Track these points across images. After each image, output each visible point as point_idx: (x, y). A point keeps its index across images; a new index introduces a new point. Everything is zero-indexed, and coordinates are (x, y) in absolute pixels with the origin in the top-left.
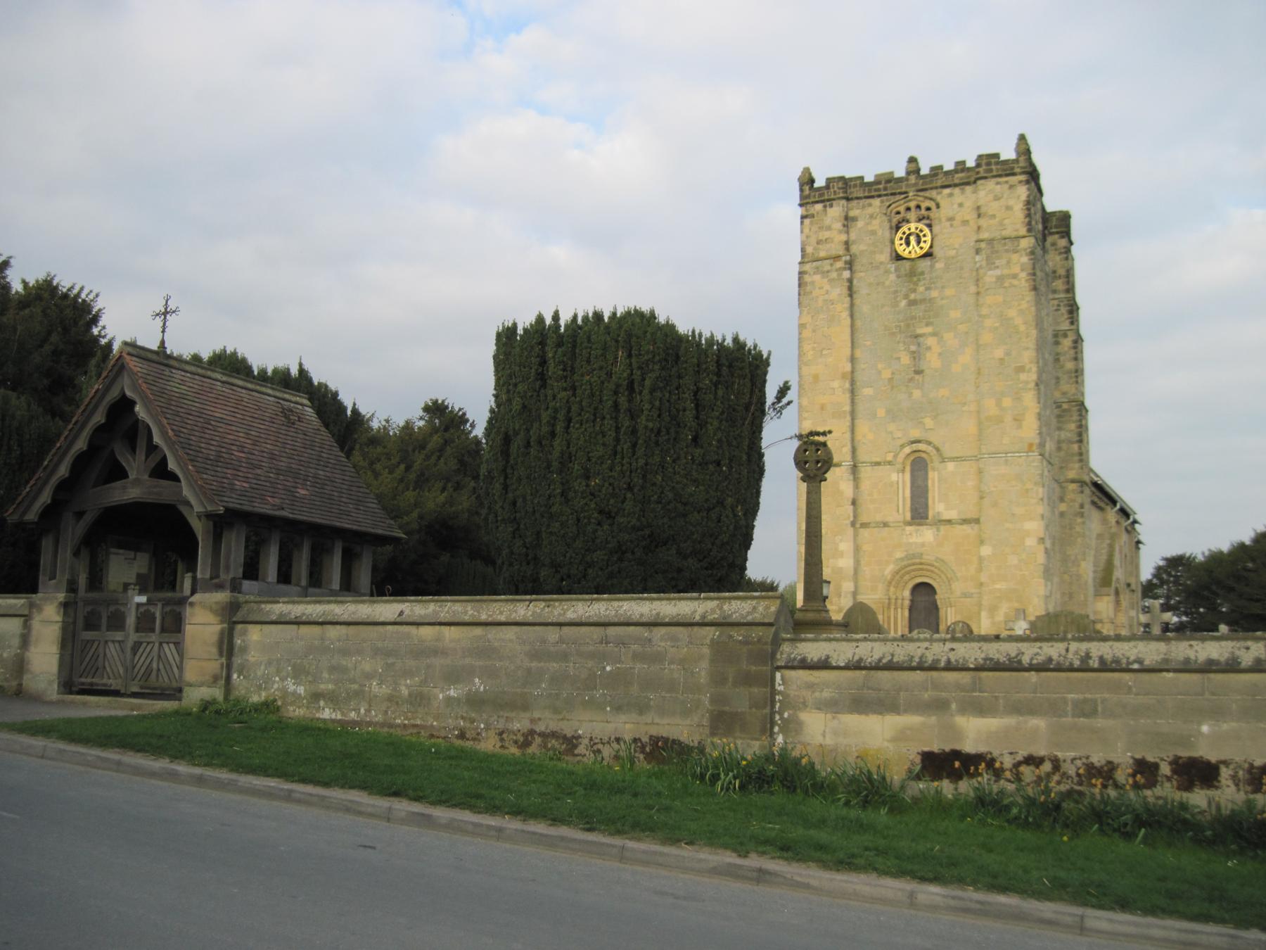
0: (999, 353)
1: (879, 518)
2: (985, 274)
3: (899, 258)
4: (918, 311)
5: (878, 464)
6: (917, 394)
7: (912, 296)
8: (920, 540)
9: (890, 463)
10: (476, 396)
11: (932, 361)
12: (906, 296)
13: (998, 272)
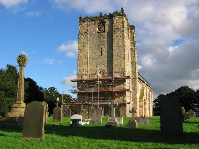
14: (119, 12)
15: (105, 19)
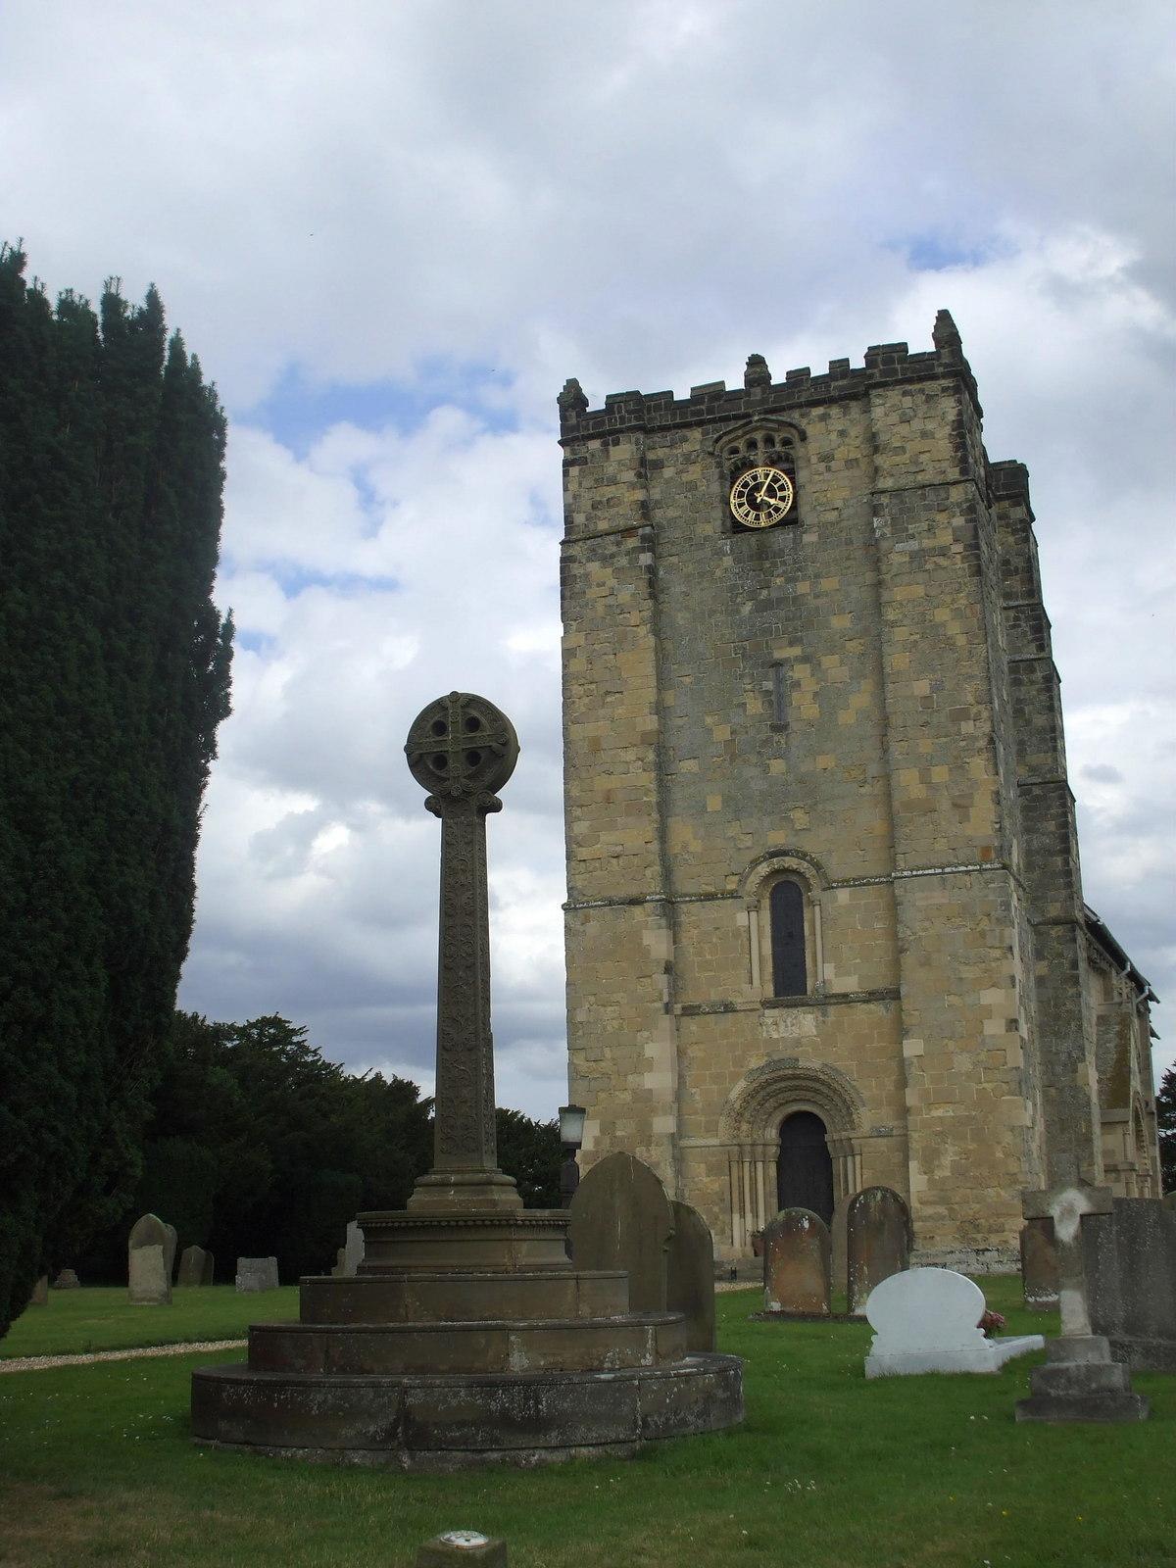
3: (737, 528)
5: (710, 897)
9: (733, 895)
11: (804, 706)
12: (752, 596)
13: (914, 545)
14: (921, 342)
15: (791, 407)
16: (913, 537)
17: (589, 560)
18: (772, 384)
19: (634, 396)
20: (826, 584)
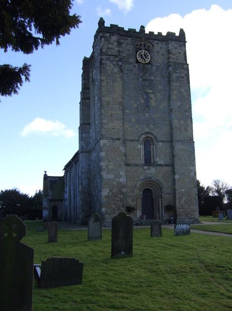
0: (179, 104)
1: (134, 162)
2: (173, 74)
3: (137, 62)
4: (147, 83)
5: (133, 141)
6: (147, 115)
7: (144, 78)
8: (150, 172)
9: (138, 141)
10: (109, 26)
11: (153, 103)
12: (142, 77)
13: (177, 75)
16: (177, 73)
17: (107, 60)
18: (178, 35)
19: (117, 26)
20: (157, 79)
